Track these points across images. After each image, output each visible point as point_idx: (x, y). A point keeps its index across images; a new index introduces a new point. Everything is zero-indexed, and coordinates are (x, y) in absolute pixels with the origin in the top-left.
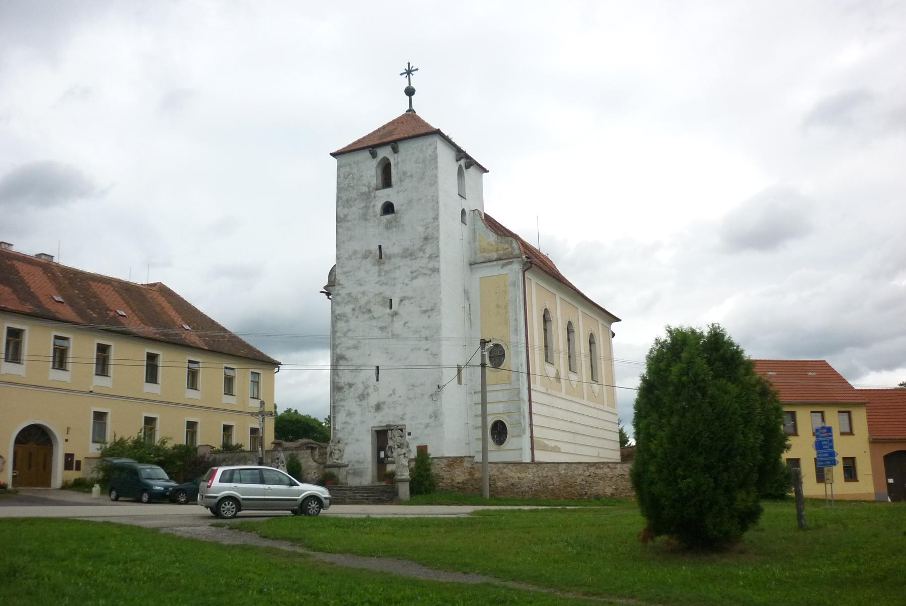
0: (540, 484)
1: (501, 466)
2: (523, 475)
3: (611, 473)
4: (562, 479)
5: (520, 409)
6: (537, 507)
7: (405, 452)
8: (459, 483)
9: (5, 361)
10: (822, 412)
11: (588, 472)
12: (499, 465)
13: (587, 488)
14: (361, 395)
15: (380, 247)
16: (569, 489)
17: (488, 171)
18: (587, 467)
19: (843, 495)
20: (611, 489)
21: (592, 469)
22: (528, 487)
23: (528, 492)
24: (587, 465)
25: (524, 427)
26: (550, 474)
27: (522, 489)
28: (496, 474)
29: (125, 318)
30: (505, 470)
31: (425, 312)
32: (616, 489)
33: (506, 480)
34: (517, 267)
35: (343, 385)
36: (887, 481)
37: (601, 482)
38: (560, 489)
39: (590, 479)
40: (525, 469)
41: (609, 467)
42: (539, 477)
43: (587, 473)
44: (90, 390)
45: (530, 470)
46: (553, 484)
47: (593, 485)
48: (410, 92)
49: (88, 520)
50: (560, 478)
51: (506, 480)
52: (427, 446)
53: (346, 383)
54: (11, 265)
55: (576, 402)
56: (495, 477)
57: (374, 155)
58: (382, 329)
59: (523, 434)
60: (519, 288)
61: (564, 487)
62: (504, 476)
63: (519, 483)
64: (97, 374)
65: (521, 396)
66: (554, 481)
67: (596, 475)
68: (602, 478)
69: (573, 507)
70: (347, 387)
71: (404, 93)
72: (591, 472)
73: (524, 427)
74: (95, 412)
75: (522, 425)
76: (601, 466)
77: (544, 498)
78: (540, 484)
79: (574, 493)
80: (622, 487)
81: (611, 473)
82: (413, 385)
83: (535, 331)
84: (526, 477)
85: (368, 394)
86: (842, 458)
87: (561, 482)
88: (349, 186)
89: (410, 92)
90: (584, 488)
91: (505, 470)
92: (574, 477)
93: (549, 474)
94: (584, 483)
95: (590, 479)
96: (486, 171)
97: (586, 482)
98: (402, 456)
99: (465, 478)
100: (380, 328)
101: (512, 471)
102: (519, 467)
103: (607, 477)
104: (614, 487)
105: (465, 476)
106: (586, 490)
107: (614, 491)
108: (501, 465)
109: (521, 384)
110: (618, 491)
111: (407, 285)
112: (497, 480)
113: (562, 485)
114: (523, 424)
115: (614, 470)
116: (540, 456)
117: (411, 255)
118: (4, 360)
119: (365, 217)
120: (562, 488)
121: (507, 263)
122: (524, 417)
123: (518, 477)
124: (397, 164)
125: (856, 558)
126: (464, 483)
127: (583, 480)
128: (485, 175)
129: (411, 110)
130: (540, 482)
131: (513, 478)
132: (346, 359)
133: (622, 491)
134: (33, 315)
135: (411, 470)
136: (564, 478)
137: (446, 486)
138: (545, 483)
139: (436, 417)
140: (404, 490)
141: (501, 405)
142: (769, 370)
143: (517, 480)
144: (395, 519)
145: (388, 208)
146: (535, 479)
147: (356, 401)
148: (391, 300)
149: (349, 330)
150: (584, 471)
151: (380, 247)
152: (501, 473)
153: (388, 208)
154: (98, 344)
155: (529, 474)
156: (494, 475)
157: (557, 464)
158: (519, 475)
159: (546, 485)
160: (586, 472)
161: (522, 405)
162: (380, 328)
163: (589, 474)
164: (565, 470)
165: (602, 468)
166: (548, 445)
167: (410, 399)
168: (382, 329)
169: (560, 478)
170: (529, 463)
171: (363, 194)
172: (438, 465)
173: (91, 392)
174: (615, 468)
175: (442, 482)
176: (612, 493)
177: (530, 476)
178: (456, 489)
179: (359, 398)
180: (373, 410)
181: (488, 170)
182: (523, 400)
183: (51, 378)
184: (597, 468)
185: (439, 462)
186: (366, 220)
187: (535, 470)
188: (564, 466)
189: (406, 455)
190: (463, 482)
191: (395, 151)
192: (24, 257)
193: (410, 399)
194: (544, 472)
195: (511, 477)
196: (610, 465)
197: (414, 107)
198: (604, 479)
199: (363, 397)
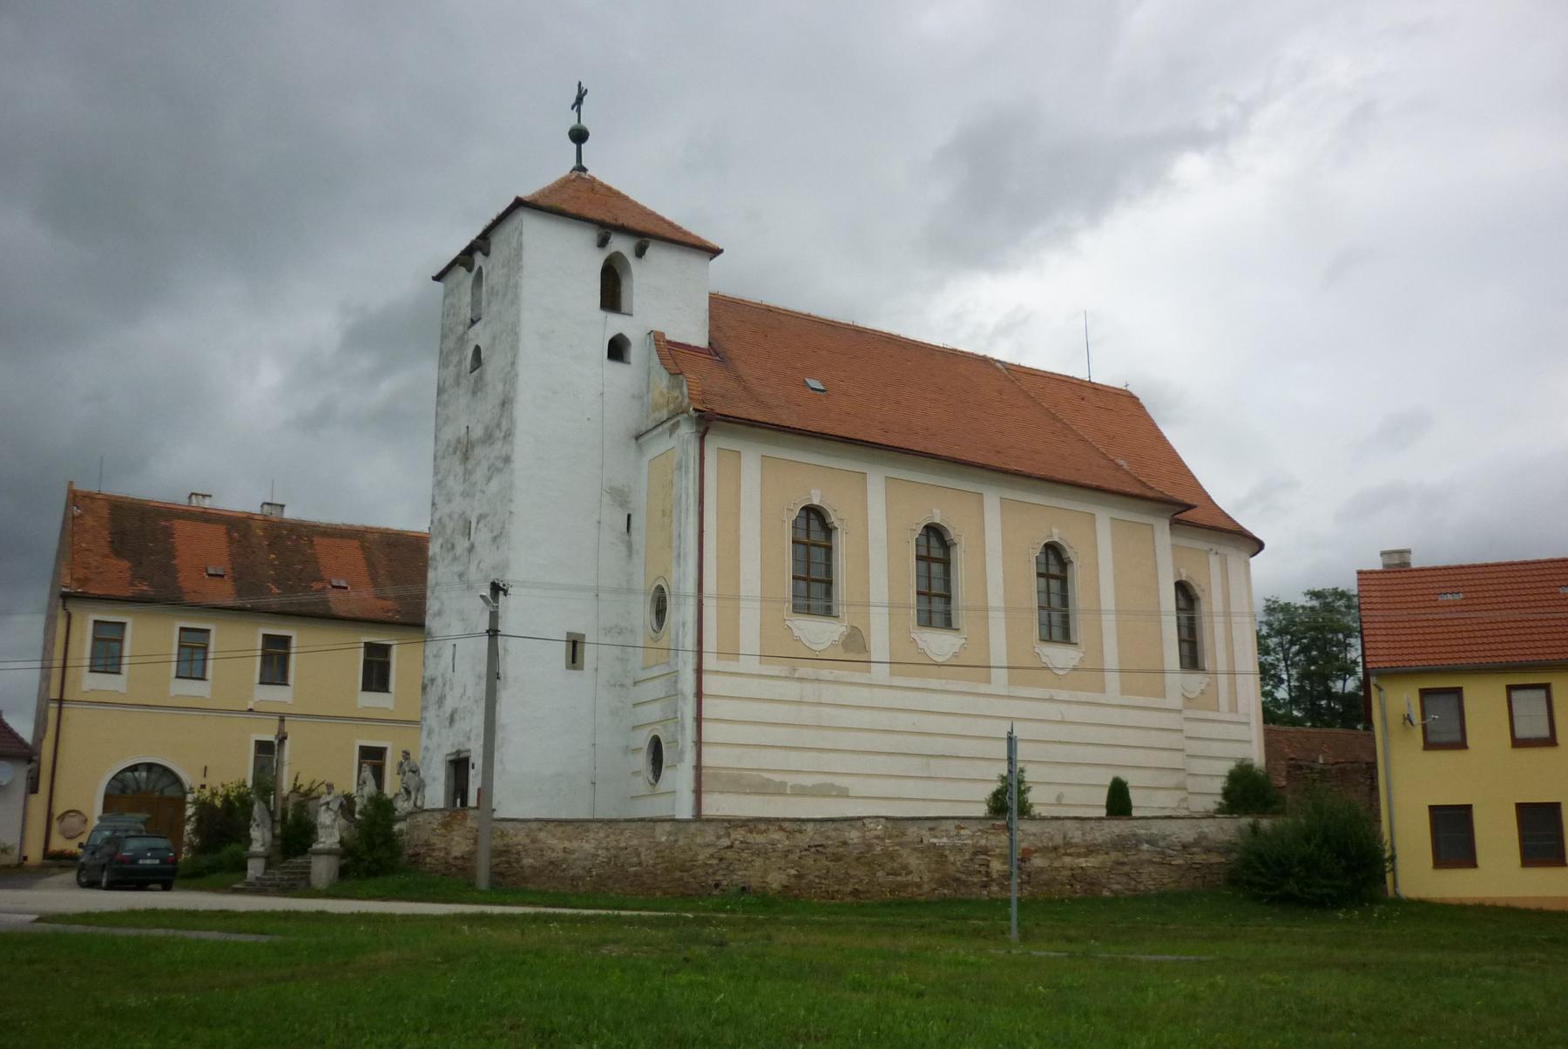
0: (608, 863)
1: (534, 826)
2: (575, 844)
3: (787, 842)
4: (660, 854)
5: (676, 712)
6: (554, 910)
8: (456, 858)
9: (91, 671)
10: (1546, 687)
11: (727, 840)
12: (529, 824)
13: (721, 872)
16: (678, 874)
18: (727, 828)
19: (1518, 899)
20: (784, 876)
21: (738, 835)
22: (584, 868)
23: (581, 878)
24: (726, 824)
25: (681, 749)
26: (635, 842)
27: (571, 873)
28: (522, 842)
29: (343, 590)
30: (542, 834)
32: (799, 876)
33: (540, 853)
34: (686, 431)
37: (759, 862)
38: (656, 875)
39: (729, 854)
40: (580, 833)
41: (781, 829)
42: (608, 849)
43: (726, 842)
44: (249, 707)
45: (591, 835)
46: (640, 864)
47: (736, 866)
48: (579, 136)
50: (657, 852)
51: (540, 853)
54: (167, 527)
55: (949, 692)
56: (519, 847)
57: (603, 243)
59: (679, 762)
60: (687, 472)
61: (666, 869)
62: (537, 845)
63: (565, 860)
64: (262, 683)
65: (679, 686)
66: (643, 857)
67: (746, 845)
68: (762, 852)
69: (604, 912)
71: (568, 136)
72: (736, 840)
73: (681, 749)
74: (257, 742)
75: (677, 746)
76: (762, 827)
77: (619, 891)
78: (608, 863)
79: (688, 883)
80: (817, 873)
81: (787, 842)
83: (872, 555)
84: (582, 847)
86: (1427, 809)
87: (659, 860)
89: (579, 136)
90: (714, 873)
91: (542, 835)
92: (690, 849)
93: (631, 843)
94: (714, 862)
95: (729, 854)
97: (721, 860)
98: (323, 808)
99: (467, 849)
101: (554, 836)
102: (569, 828)
103: (774, 851)
104: (793, 872)
105: (467, 846)
106: (718, 878)
107: (792, 880)
108: (535, 823)
109: (680, 664)
110: (804, 881)
112: (523, 853)
113: (659, 867)
114: (679, 741)
115: (798, 835)
116: (719, 805)
118: (88, 669)
120: (659, 872)
121: (673, 425)
122: (683, 728)
123: (565, 848)
126: (466, 859)
127: (712, 856)
129: (580, 168)
130: (610, 859)
131: (553, 851)
133: (817, 880)
134: (131, 599)
135: (1240, 817)
136: (667, 851)
137: (436, 863)
138: (622, 860)
140: (322, 870)
141: (658, 705)
142: (1443, 591)
143: (561, 854)
146: (600, 852)
150: (719, 837)
152: (534, 841)
154: (264, 635)
155: (587, 842)
156: (518, 845)
157: (651, 824)
158: (567, 844)
159: (623, 866)
160: (722, 840)
161: (680, 703)
163: (729, 843)
164: (669, 834)
165: (765, 831)
166: (786, 784)
169: (657, 852)
170: (687, 821)
172: (429, 823)
173: (251, 710)
174: (800, 832)
175: (430, 856)
176: (785, 883)
177: (588, 847)
178: (454, 869)
182: (682, 694)
183: (85, 687)
184: (751, 832)
185: (431, 819)
187: (602, 834)
188: (667, 827)
189: (331, 806)
190: (462, 857)
191: (640, 252)
192: (203, 512)
194: (623, 838)
195: (549, 848)
196: (786, 825)
197: (584, 163)
198: (766, 853)
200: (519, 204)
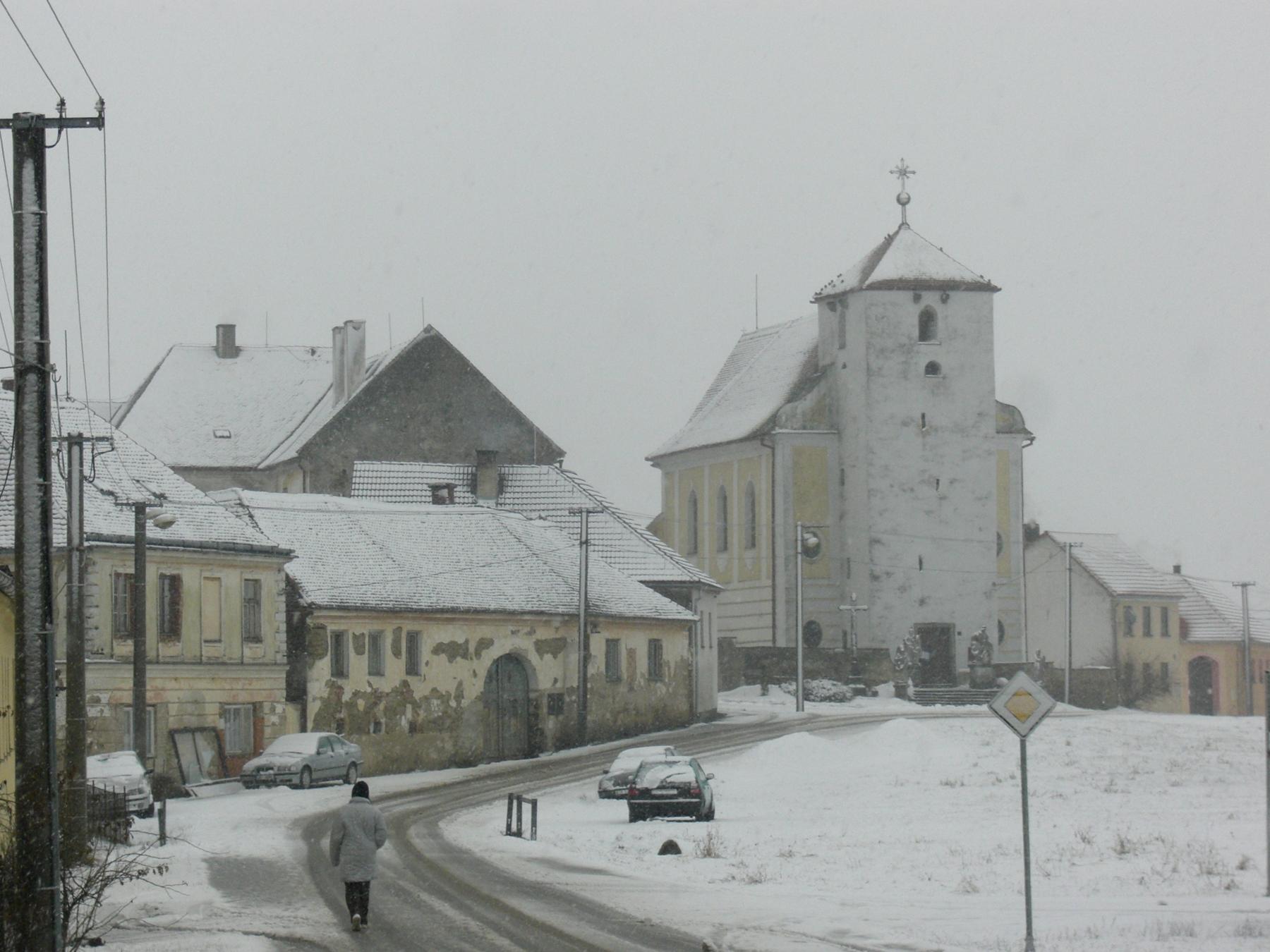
7: (57, 447)
15: (923, 416)
17: (1000, 290)
31: (980, 499)
48: (903, 202)
49: (659, 731)
57: (917, 298)
58: (928, 513)
89: (903, 202)
119: (905, 375)
125: (897, 668)
128: (996, 296)
132: (883, 544)
144: (290, 646)
145: (932, 368)
148: (938, 480)
151: (923, 416)
153: (932, 368)
168: (928, 513)
171: (902, 346)
179: (899, 589)
181: (999, 287)
186: (906, 378)
191: (944, 300)
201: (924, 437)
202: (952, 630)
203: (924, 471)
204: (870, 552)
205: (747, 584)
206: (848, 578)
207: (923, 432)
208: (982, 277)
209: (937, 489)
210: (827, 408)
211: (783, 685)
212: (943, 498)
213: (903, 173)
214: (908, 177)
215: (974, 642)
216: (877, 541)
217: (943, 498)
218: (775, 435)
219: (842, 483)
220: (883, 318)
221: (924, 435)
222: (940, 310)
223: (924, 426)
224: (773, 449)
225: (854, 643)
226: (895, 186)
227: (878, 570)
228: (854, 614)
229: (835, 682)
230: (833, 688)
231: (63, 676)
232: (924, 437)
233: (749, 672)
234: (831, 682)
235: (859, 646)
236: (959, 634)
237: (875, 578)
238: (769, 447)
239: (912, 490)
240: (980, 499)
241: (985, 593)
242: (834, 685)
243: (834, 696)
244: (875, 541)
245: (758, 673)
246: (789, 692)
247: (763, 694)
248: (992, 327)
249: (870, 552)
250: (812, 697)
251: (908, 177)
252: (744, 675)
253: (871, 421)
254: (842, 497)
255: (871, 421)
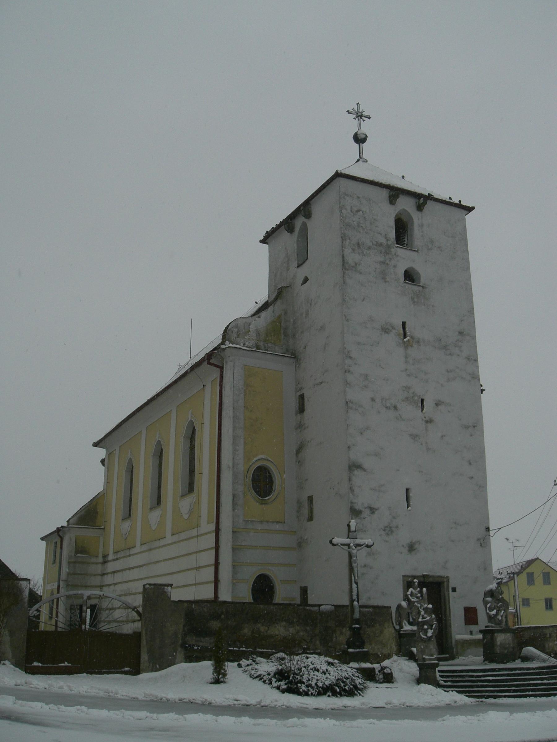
14: (387, 527)
15: (404, 324)
17: (473, 208)
31: (467, 427)
35: (361, 509)
36: (55, 598)
52: (465, 608)
53: (366, 506)
57: (392, 200)
58: (414, 437)
70: (368, 512)
82: (455, 523)
85: (397, 527)
88: (359, 226)
89: (359, 139)
96: (470, 209)
100: (411, 435)
111: (442, 385)
117: (445, 347)
124: (421, 226)
128: (470, 218)
132: (364, 470)
139: (485, 569)
147: (381, 535)
148: (422, 401)
149: (368, 428)
151: (404, 324)
162: (411, 435)
167: (453, 541)
168: (414, 437)
179: (384, 530)
180: (405, 551)
191: (420, 208)
193: (453, 541)
199: (389, 530)
200: (338, 175)
201: (406, 348)
202: (445, 584)
203: (408, 388)
204: (350, 479)
205: (183, 536)
206: (310, 518)
207: (404, 342)
208: (450, 198)
209: (422, 410)
210: (282, 331)
211: (244, 662)
212: (429, 421)
213: (360, 116)
214: (364, 121)
215: (489, 599)
216: (359, 467)
217: (429, 421)
218: (224, 349)
219: (301, 409)
220: (358, 211)
221: (407, 345)
222: (416, 217)
223: (405, 336)
224: (221, 368)
225: (355, 597)
226: (352, 126)
227: (361, 502)
228: (354, 552)
229: (330, 660)
230: (330, 668)
231: (417, 605)
232: (406, 348)
233: (191, 640)
234: (323, 659)
235: (363, 601)
236: (454, 590)
237: (355, 513)
238: (216, 366)
239: (395, 408)
240: (467, 427)
241: (478, 540)
242: (329, 664)
243: (337, 685)
244: (354, 466)
245: (207, 642)
246: (259, 677)
247: (217, 681)
248: (466, 245)
249: (350, 479)
250: (303, 688)
251: (364, 121)
252: (183, 646)
253: (347, 320)
254: (300, 426)
255: (347, 320)
